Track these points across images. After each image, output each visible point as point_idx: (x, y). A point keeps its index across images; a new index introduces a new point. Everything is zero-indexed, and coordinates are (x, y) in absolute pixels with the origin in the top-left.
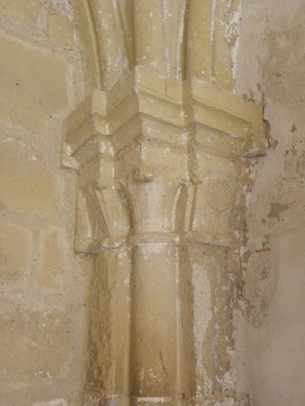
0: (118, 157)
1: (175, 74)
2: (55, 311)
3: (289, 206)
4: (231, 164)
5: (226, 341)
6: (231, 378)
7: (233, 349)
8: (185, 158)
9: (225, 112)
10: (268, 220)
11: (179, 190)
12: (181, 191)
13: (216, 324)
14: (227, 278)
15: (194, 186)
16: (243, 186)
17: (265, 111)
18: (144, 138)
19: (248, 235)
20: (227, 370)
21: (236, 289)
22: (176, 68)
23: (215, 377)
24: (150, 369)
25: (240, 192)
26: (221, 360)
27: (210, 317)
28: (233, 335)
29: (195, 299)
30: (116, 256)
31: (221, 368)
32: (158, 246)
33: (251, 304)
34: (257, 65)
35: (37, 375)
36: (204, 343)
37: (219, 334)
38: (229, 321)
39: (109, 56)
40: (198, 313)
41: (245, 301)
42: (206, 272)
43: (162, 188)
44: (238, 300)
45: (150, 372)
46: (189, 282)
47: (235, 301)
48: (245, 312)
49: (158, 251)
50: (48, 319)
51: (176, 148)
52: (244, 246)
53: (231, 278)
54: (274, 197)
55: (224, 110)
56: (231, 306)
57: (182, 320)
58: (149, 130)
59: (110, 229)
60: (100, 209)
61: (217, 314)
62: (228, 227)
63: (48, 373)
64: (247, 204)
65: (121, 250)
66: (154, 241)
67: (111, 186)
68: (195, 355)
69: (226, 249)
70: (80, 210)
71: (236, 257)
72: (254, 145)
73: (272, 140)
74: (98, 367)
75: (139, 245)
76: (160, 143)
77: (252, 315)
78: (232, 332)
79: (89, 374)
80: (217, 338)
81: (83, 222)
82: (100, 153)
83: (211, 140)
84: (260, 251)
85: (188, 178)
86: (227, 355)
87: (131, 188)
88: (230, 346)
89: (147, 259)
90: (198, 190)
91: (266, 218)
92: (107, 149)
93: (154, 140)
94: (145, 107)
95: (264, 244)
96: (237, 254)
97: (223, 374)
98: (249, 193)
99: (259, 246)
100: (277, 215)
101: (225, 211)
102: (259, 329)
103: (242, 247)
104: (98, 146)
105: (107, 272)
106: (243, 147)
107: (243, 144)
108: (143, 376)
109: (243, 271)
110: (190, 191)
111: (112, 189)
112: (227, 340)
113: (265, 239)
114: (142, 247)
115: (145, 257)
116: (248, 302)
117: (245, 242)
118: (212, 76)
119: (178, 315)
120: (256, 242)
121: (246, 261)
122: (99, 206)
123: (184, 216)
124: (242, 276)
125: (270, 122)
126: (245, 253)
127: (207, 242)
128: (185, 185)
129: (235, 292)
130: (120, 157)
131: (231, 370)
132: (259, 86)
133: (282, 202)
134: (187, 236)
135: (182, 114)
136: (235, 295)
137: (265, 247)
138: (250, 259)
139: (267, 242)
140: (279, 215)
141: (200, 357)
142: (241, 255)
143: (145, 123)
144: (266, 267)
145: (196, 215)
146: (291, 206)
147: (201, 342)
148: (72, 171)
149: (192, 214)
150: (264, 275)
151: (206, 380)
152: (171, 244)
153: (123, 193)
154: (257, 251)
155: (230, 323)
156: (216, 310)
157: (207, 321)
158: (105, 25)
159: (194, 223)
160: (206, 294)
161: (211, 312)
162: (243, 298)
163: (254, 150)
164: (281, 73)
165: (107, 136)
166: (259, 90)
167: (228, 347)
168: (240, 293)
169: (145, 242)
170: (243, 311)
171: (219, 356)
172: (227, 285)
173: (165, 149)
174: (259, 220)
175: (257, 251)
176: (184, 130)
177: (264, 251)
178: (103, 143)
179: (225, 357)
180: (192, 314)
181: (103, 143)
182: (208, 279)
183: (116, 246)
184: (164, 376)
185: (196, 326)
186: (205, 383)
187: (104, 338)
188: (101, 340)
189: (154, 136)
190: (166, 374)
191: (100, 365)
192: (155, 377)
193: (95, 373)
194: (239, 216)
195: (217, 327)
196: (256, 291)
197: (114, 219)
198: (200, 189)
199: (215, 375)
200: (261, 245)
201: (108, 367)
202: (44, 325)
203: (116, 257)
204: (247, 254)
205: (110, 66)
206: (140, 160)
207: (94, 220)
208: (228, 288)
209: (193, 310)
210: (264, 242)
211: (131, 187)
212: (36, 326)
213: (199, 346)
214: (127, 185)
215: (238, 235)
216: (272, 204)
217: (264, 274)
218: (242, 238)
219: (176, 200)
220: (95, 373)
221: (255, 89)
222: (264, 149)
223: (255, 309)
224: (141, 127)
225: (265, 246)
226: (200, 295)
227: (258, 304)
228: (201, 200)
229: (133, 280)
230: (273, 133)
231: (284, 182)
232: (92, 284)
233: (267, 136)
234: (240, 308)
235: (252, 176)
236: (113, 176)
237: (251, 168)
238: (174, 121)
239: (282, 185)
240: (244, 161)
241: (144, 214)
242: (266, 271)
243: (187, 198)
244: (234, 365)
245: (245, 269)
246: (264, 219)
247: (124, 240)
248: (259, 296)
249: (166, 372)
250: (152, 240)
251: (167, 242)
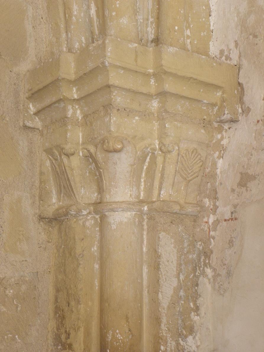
0: (86, 122)
1: (147, 27)
2: (22, 278)
3: (256, 177)
4: (203, 131)
5: (191, 307)
6: (194, 341)
7: (198, 315)
8: (156, 125)
9: (196, 79)
11: (149, 157)
12: (150, 159)
13: (182, 291)
14: (194, 246)
15: (163, 154)
16: (215, 153)
17: (241, 72)
18: (113, 108)
19: (217, 204)
20: (191, 334)
21: (203, 258)
22: (148, 20)
23: (179, 340)
24: (117, 331)
25: (211, 159)
26: (185, 324)
27: (175, 283)
28: (198, 302)
29: (161, 266)
30: (83, 224)
31: (184, 332)
32: (126, 215)
33: (217, 273)
34: (236, 19)
35: (7, 338)
36: (169, 307)
37: (184, 301)
38: (195, 288)
39: (75, 4)
40: (163, 280)
41: (212, 270)
42: (173, 240)
43: (131, 157)
44: (205, 268)
45: (117, 334)
47: (201, 269)
48: (212, 280)
49: (125, 220)
50: (15, 285)
51: (146, 115)
52: (213, 215)
53: (198, 246)
54: (243, 166)
55: (195, 77)
56: (197, 274)
57: (148, 287)
58: (118, 100)
59: (77, 197)
60: (67, 175)
61: (183, 281)
62: (197, 196)
63: (17, 336)
64: (218, 171)
65: (88, 218)
66: (122, 211)
67: (79, 152)
68: (160, 318)
69: (195, 218)
70: (44, 174)
71: (204, 226)
72: (226, 112)
73: (245, 106)
74: (66, 331)
75: (107, 213)
76: (128, 112)
77: (218, 283)
78: (197, 298)
79: (57, 338)
80: (182, 303)
81: (47, 187)
82: (67, 118)
83: (181, 107)
84: (228, 220)
85: (157, 147)
86: (192, 321)
87: (100, 156)
88: (194, 312)
89: (115, 228)
90: (167, 160)
91: (235, 187)
92: (74, 113)
93: (123, 110)
94: (115, 78)
95: (232, 213)
96: (206, 222)
97: (186, 337)
98: (221, 159)
99: (228, 216)
101: (195, 180)
102: (223, 296)
103: (211, 215)
104: (65, 109)
105: (75, 239)
106: (215, 111)
107: (216, 109)
108: (110, 337)
109: (212, 240)
110: (160, 160)
111: (79, 156)
112: (192, 306)
113: (233, 209)
114: (111, 216)
115: (112, 226)
116: (214, 270)
117: (214, 210)
118: (187, 30)
119: (145, 283)
120: (225, 211)
121: (215, 230)
122: (66, 172)
123: (153, 185)
124: (211, 245)
125: (244, 85)
127: (175, 211)
128: (154, 153)
129: (202, 260)
130: (88, 123)
131: (194, 334)
133: (250, 172)
134: (155, 205)
135: (152, 81)
136: (202, 263)
137: (233, 217)
139: (235, 212)
140: (248, 185)
141: (164, 320)
142: (210, 223)
143: (114, 94)
144: (233, 236)
146: (259, 177)
147: (166, 307)
148: (34, 131)
149: (161, 184)
150: (231, 244)
151: (169, 341)
152: (138, 213)
153: (90, 158)
154: (225, 220)
155: (196, 290)
156: (182, 277)
157: (172, 287)
159: (162, 192)
160: (172, 262)
161: (176, 279)
162: (210, 266)
163: (227, 116)
164: (257, 34)
165: (74, 100)
166: (236, 48)
167: (193, 313)
168: (207, 261)
169: (113, 210)
170: (209, 280)
171: (183, 321)
172: (194, 254)
173: (134, 117)
175: (225, 220)
176: (154, 97)
177: (232, 220)
178: (70, 107)
179: (189, 322)
180: (158, 281)
181: (70, 107)
182: (175, 247)
183: (83, 214)
184: (130, 337)
185: (161, 292)
186: (168, 344)
187: (73, 303)
188: (69, 306)
189: (124, 106)
190: (132, 336)
192: (122, 338)
193: (63, 337)
194: (209, 184)
195: (182, 293)
196: (222, 260)
197: (82, 187)
198: (169, 159)
199: (178, 338)
200: (229, 214)
201: (77, 330)
202: (11, 291)
203: (84, 225)
204: (217, 222)
205: (76, 16)
206: (110, 131)
207: (60, 185)
208: (195, 256)
209: (159, 277)
210: (233, 211)
211: (99, 155)
212: (5, 292)
213: (163, 311)
214: (96, 153)
215: (208, 203)
216: (241, 174)
217: (231, 243)
218: (212, 207)
219: (145, 167)
220: (63, 337)
221: (232, 46)
222: (237, 114)
223: (220, 277)
224: (111, 97)
225: (233, 215)
226: (167, 263)
227: (224, 272)
228: (170, 169)
229: (102, 247)
230: (246, 99)
231: (253, 152)
232: (58, 251)
233: (241, 101)
234: (207, 276)
235: (224, 142)
236: (81, 142)
238: (144, 90)
239: (252, 155)
240: (216, 126)
241: (113, 183)
242: (232, 241)
243: (156, 167)
244: (198, 329)
245: (214, 238)
246: (234, 188)
247: (92, 208)
248: (225, 264)
249: (132, 334)
250: (120, 210)
251: (135, 211)
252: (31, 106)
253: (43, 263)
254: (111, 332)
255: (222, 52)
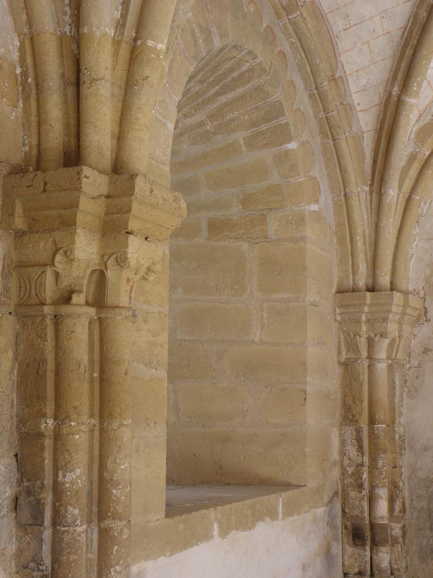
10: (422, 354)
19: (411, 359)
46: (393, 380)
64: (412, 345)
84: (416, 367)
95: (418, 364)
99: (416, 365)
100: (426, 353)
105: (359, 374)
116: (408, 389)
121: (409, 371)
126: (409, 367)
132: (423, 288)
138: (411, 370)
145: (399, 352)
154: (415, 367)
158: (360, 245)
174: (417, 353)
175: (415, 367)
187: (357, 402)
191: (354, 414)
204: (410, 368)
216: (424, 348)
217: (417, 377)
221: (421, 288)
235: (416, 332)
237: (416, 328)
245: (408, 374)
252: (337, 309)
253: (357, 386)
254: (378, 415)
255: (415, 290)
